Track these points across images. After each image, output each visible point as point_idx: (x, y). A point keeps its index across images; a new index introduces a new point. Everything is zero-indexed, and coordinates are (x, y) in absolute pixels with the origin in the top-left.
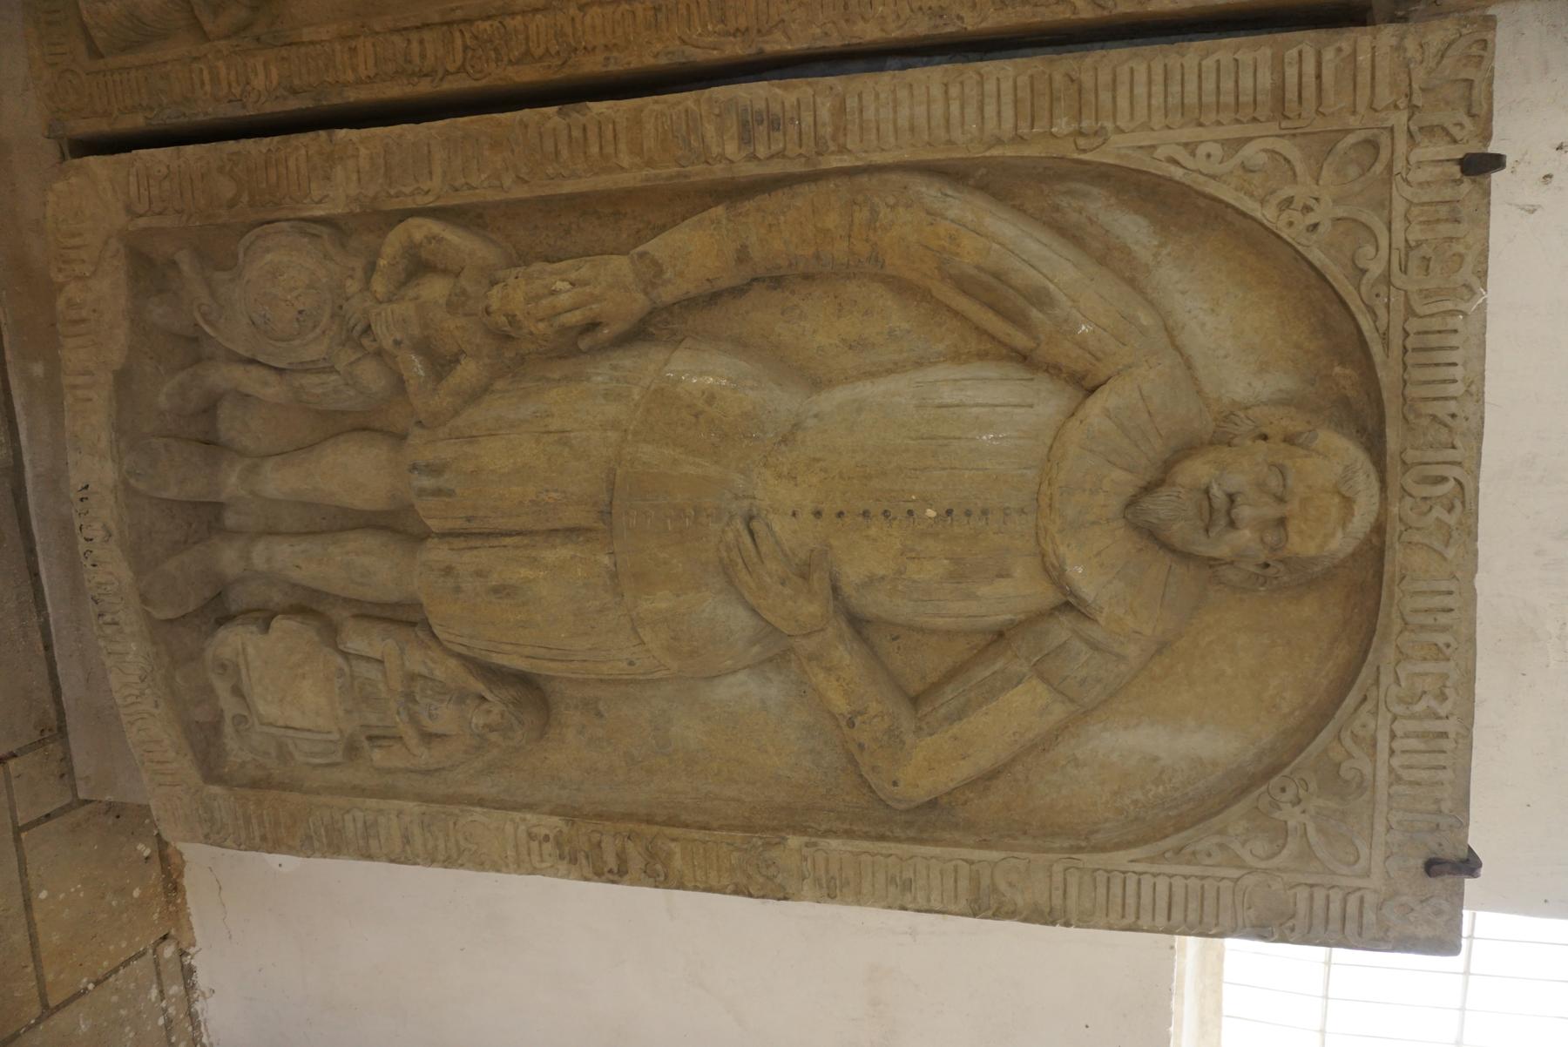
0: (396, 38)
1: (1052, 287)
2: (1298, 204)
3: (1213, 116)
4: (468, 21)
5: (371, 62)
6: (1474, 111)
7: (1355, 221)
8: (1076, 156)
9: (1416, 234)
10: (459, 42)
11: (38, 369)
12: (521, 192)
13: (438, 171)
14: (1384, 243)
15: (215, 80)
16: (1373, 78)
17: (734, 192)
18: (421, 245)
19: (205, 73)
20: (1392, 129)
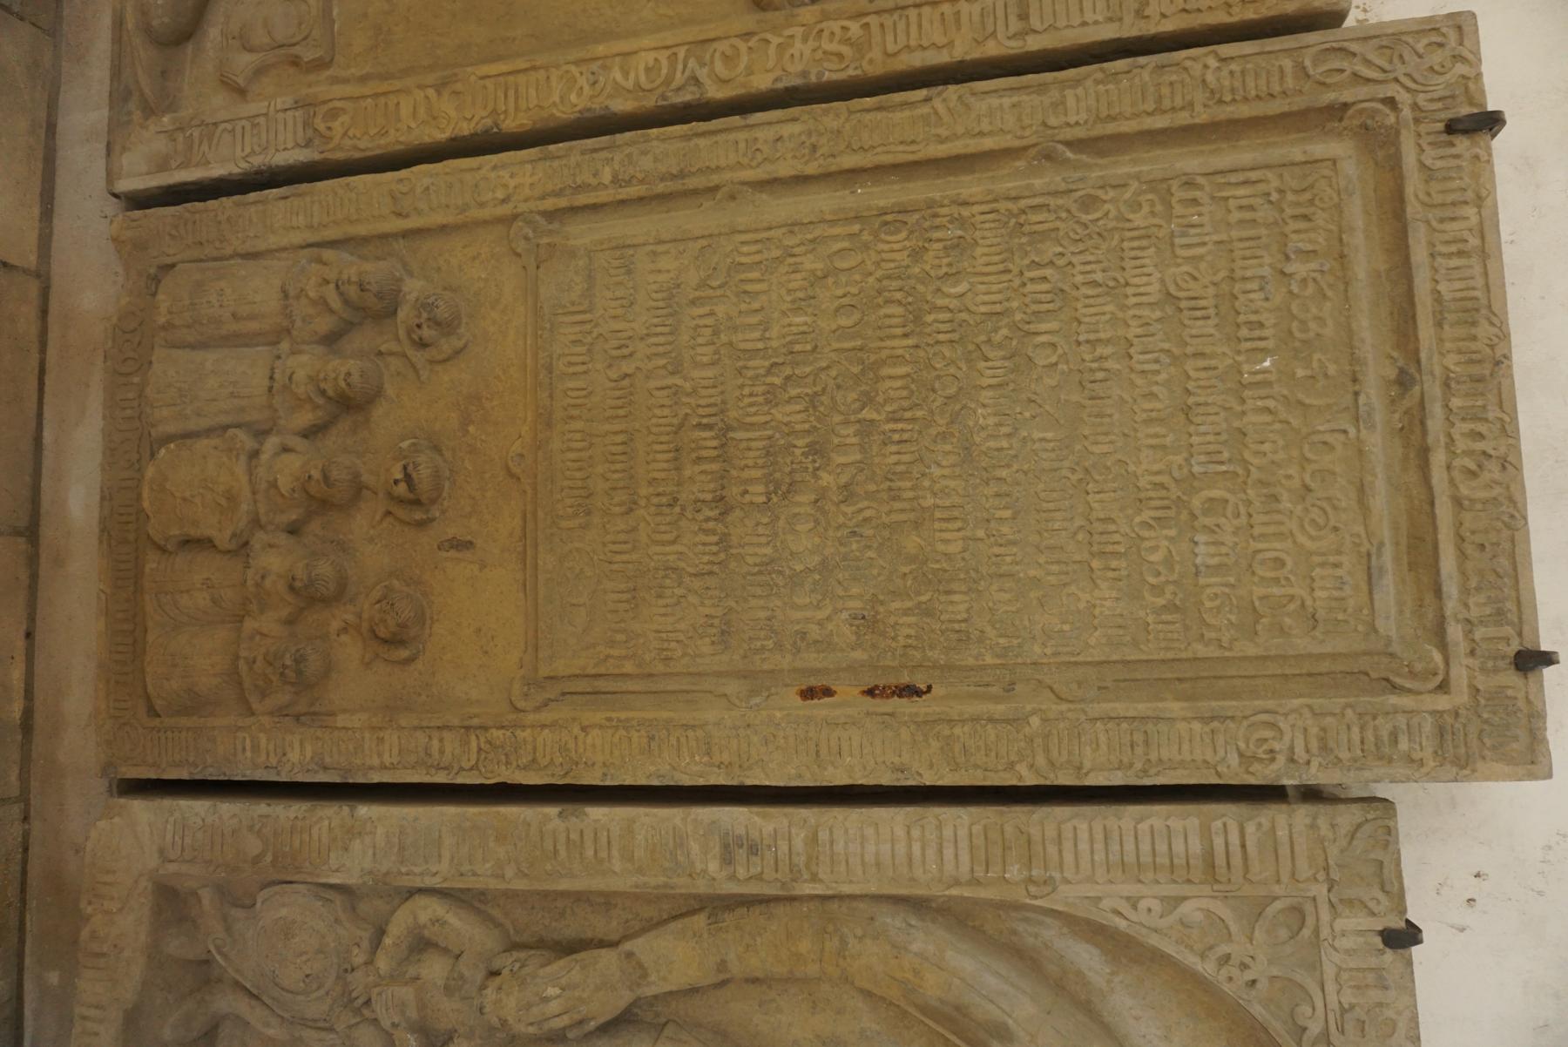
0: (419, 734)
1: (1010, 1022)
2: (1235, 960)
3: (1150, 875)
4: (485, 728)
5: (395, 751)
6: (1388, 888)
7: (1290, 980)
8: (1028, 901)
9: (1348, 998)
10: (474, 744)
11: (53, 978)
12: (521, 885)
13: (446, 854)
14: (1319, 1004)
15: (256, 748)
16: (1292, 852)
17: (719, 906)
18: (425, 926)
19: (248, 741)
20: (1314, 899)
